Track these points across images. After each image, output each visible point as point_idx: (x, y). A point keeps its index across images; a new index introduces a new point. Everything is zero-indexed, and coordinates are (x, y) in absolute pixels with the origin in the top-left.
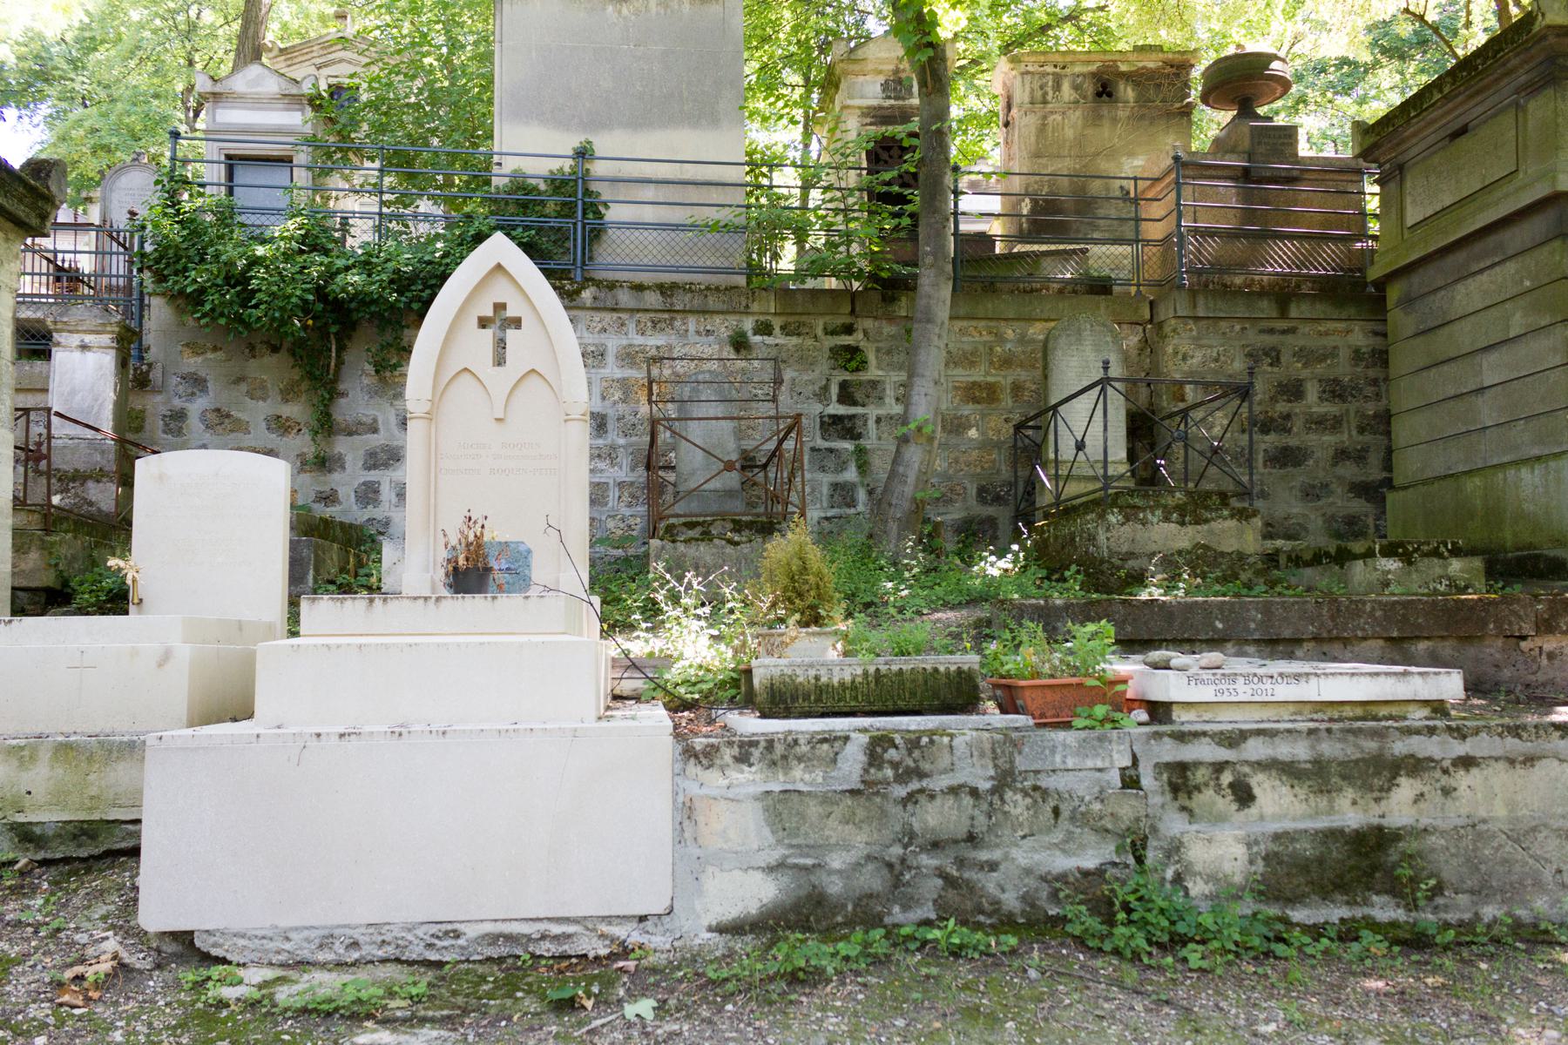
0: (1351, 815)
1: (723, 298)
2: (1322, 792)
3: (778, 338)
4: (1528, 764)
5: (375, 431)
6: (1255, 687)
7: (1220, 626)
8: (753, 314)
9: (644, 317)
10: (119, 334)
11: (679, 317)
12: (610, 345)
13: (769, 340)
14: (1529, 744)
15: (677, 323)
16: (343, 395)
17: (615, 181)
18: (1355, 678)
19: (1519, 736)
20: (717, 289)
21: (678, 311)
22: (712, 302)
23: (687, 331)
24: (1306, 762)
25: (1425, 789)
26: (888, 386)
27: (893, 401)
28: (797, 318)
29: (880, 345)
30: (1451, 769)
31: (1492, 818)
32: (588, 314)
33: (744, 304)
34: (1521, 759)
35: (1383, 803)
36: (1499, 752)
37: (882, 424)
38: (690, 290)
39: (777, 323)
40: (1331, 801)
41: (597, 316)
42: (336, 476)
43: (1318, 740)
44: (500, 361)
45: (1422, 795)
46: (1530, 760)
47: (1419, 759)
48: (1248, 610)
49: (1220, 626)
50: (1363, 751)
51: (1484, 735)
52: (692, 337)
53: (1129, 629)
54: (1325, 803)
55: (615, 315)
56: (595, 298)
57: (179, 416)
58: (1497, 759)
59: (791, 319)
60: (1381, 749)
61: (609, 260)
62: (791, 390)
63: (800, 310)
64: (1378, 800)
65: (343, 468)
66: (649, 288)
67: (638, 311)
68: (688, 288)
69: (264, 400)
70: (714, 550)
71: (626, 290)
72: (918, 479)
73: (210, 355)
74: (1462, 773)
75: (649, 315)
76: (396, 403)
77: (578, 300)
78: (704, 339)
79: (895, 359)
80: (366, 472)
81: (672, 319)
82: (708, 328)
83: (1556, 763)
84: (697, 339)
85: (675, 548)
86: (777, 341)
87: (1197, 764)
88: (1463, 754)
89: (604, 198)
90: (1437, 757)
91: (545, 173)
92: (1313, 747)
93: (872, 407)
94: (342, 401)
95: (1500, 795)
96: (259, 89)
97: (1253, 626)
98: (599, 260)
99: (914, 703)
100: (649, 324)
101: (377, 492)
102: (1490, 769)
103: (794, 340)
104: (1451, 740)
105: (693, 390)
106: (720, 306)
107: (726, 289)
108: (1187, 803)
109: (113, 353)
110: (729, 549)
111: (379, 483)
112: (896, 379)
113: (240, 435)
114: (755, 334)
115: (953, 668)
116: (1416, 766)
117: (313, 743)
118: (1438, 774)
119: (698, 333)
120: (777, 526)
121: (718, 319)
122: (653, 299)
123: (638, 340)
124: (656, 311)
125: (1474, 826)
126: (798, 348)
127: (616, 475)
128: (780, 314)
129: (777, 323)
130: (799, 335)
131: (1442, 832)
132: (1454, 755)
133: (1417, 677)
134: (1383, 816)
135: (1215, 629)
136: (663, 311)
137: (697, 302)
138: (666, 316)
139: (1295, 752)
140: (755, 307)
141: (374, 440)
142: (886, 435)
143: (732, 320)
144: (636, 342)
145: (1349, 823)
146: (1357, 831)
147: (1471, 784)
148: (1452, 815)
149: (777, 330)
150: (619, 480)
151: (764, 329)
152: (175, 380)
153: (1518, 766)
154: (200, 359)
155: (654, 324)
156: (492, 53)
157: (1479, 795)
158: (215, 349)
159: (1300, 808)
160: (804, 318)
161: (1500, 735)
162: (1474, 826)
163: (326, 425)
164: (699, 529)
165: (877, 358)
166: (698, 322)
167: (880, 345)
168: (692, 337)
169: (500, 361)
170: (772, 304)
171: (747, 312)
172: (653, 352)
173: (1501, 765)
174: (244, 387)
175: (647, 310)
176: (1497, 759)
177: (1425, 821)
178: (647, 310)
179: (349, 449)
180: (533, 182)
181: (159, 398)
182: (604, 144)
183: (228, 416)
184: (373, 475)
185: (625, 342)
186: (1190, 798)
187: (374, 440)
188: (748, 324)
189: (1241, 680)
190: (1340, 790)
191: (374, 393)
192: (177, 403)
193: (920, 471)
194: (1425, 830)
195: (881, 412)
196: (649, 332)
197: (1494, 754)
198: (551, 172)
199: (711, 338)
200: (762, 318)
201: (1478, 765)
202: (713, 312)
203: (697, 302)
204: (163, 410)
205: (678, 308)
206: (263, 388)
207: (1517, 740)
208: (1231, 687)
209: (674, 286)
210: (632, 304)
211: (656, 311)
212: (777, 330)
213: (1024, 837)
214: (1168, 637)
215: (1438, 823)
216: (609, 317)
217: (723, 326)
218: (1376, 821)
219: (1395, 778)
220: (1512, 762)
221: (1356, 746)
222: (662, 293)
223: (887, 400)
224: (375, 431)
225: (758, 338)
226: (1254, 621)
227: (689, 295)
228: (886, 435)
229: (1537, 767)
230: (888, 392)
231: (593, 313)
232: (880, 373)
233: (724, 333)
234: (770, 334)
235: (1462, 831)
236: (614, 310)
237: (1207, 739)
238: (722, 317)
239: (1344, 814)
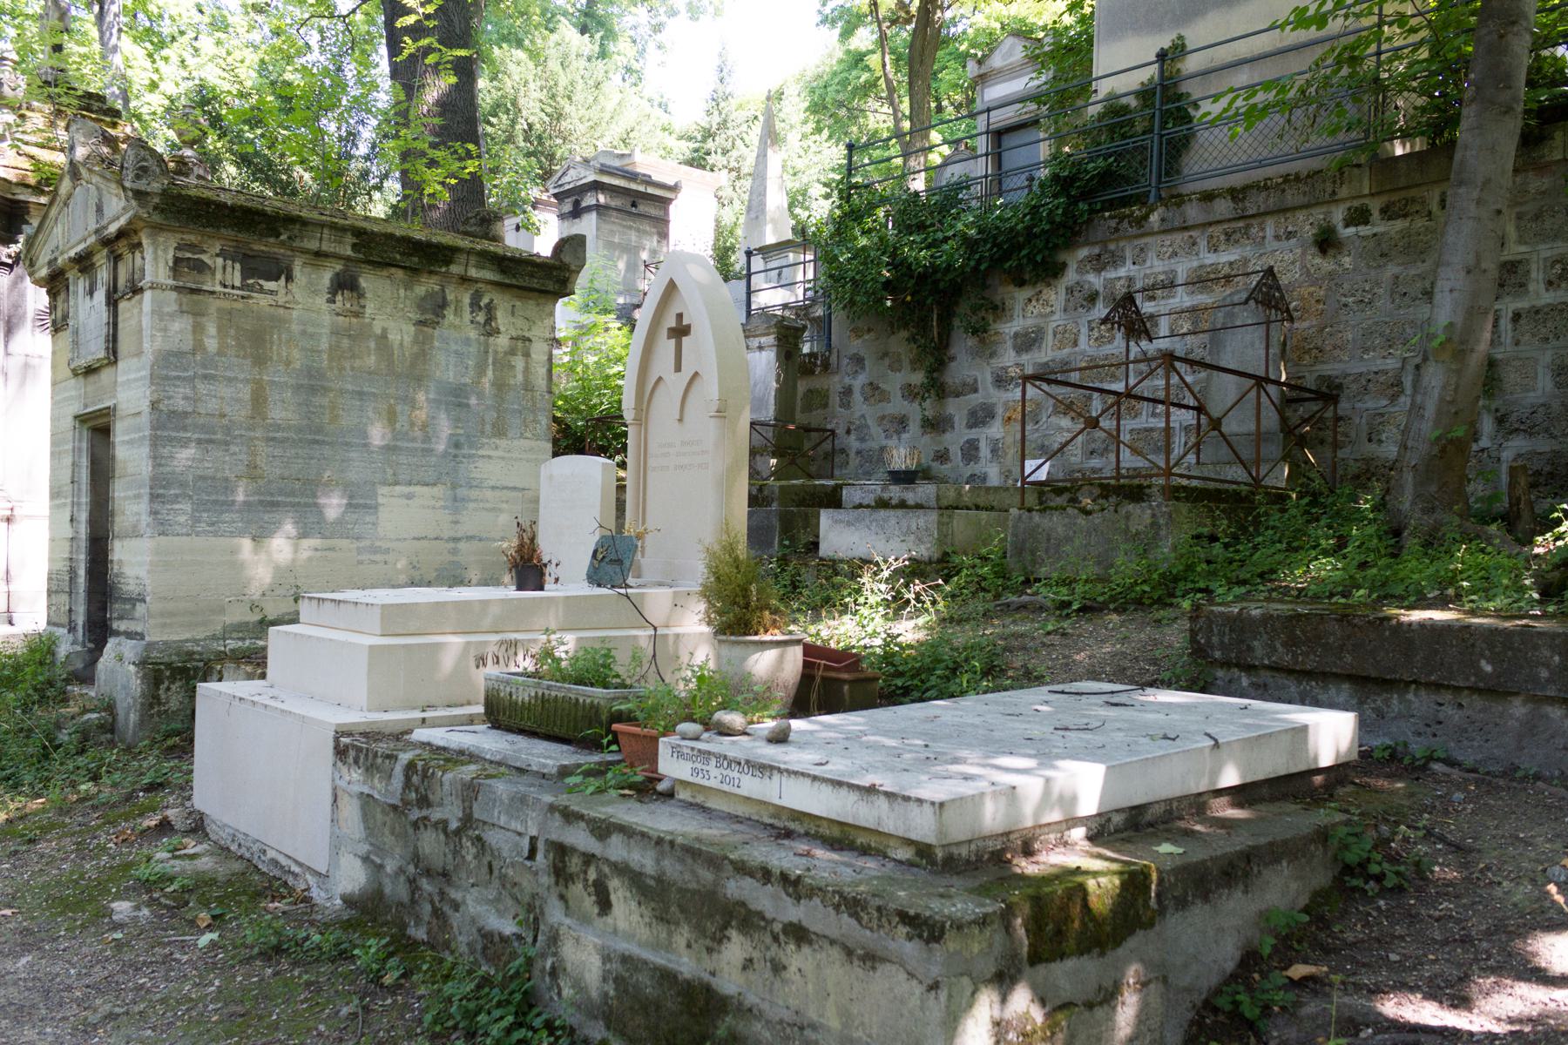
0: (685, 959)
1: (1303, 188)
2: (662, 919)
3: (1379, 226)
4: (869, 964)
5: (976, 391)
6: (725, 773)
7: (1489, 668)
8: (1343, 200)
9: (1217, 231)
10: (778, 333)
11: (1254, 222)
12: (1179, 270)
13: (1364, 230)
14: (868, 933)
15: (1254, 231)
16: (952, 359)
17: (1205, 73)
18: (817, 784)
19: (855, 915)
20: (1297, 178)
21: (1253, 216)
22: (1292, 197)
23: (1264, 238)
24: (652, 877)
25: (756, 955)
26: (1534, 267)
27: (1542, 286)
28: (1403, 194)
29: (1524, 209)
30: (782, 937)
31: (822, 1026)
32: (1159, 238)
33: (1329, 190)
34: (860, 952)
35: (715, 956)
36: (834, 933)
37: (1522, 322)
38: (1266, 188)
39: (1375, 205)
40: (670, 934)
41: (1168, 239)
42: (948, 436)
43: (662, 854)
44: (678, 368)
45: (751, 960)
46: (871, 959)
47: (749, 911)
48: (1536, 647)
49: (1489, 668)
50: (698, 882)
51: (817, 901)
52: (1271, 244)
53: (1349, 658)
54: (664, 935)
55: (1186, 234)
56: (1163, 220)
57: (848, 391)
58: (832, 942)
59: (1395, 197)
60: (716, 884)
61: (1196, 168)
62: (1393, 292)
63: (1402, 182)
64: (710, 950)
65: (953, 427)
66: (1219, 195)
67: (1210, 224)
68: (1263, 187)
69: (900, 371)
70: (1067, 520)
71: (1195, 202)
72: (1439, 413)
73: (866, 337)
74: (793, 947)
75: (1220, 228)
76: (993, 361)
77: (1146, 225)
78: (1285, 244)
79: (1547, 225)
80: (967, 431)
81: (1248, 227)
82: (1290, 229)
83: (903, 976)
84: (1276, 245)
85: (1031, 518)
86: (1375, 230)
87: (573, 850)
88: (795, 920)
89: (1194, 97)
90: (769, 916)
91: (1135, 86)
92: (658, 861)
93: (1508, 299)
94: (953, 364)
95: (832, 996)
96: (1012, 59)
97: (1544, 674)
98: (1186, 171)
99: (562, 732)
100: (1222, 237)
101: (977, 449)
102: (824, 954)
103: (1399, 224)
104: (784, 895)
105: (1227, 315)
106: (1301, 200)
107: (1308, 176)
108: (564, 892)
109: (775, 349)
110: (1081, 520)
111: (978, 440)
112: (1549, 254)
113: (884, 404)
114: (1347, 226)
115: (588, 701)
116: (748, 920)
117: (236, 702)
118: (768, 940)
119: (1277, 238)
120: (1147, 491)
121: (1301, 215)
122: (1223, 207)
123: (1210, 259)
124: (1229, 220)
125: (802, 1028)
126: (1405, 234)
127: (1182, 418)
128: (1379, 193)
129: (1375, 205)
130: (1405, 216)
131: (768, 1022)
132: (786, 920)
133: (882, 798)
134: (713, 974)
135: (1479, 672)
136: (1234, 219)
137: (1273, 201)
138: (1241, 224)
139: (644, 861)
140: (1344, 192)
141: (975, 399)
142: (1527, 337)
143: (1318, 214)
144: (1208, 262)
145: (682, 969)
146: (688, 982)
147: (802, 967)
148: (781, 1003)
149: (1376, 214)
150: (1185, 424)
151: (1359, 217)
152: (846, 361)
153: (856, 962)
154: (860, 341)
155: (1228, 235)
156: (72, 260)
157: (810, 986)
158: (869, 330)
159: (644, 933)
160: (1413, 193)
161: (837, 907)
162: (802, 1028)
163: (937, 388)
164: (1066, 496)
165: (1518, 228)
166: (1277, 225)
167: (1524, 209)
168: (1271, 244)
169: (678, 368)
170: (1366, 183)
171: (1333, 200)
172: (1227, 270)
173: (836, 953)
174: (887, 361)
175: (1219, 222)
176: (832, 942)
177: (751, 999)
178: (1219, 222)
179: (957, 409)
180: (1124, 101)
181: (836, 378)
182: (1196, 34)
183: (878, 388)
184: (973, 434)
185: (1195, 264)
186: (567, 887)
187: (975, 399)
188: (1338, 215)
189: (713, 761)
190: (677, 924)
191: (976, 353)
192: (847, 380)
193: (1442, 400)
194: (750, 1010)
195: (1522, 304)
196: (1222, 247)
197: (827, 932)
198: (1142, 83)
199: (1293, 241)
200: (1356, 203)
201: (810, 943)
202: (1294, 209)
203: (1273, 201)
204: (839, 388)
205: (1251, 212)
206: (899, 361)
207: (853, 922)
208: (704, 767)
209: (1246, 189)
210: (1201, 219)
211: (1229, 220)
212: (1376, 214)
213: (473, 885)
214: (1406, 677)
215: (765, 1006)
216: (1179, 238)
217: (1306, 225)
218: (706, 977)
219: (726, 928)
220: (849, 953)
221: (693, 872)
222: (1233, 198)
223: (1532, 287)
224: (976, 391)
225: (1351, 230)
226: (1547, 666)
227: (1264, 194)
228: (1527, 337)
229: (878, 973)
230: (1534, 275)
231: (1163, 237)
232: (1523, 249)
233: (1309, 232)
234: (1366, 223)
235: (788, 1030)
236: (1186, 229)
237: (583, 825)
238: (1305, 212)
239: (680, 956)
